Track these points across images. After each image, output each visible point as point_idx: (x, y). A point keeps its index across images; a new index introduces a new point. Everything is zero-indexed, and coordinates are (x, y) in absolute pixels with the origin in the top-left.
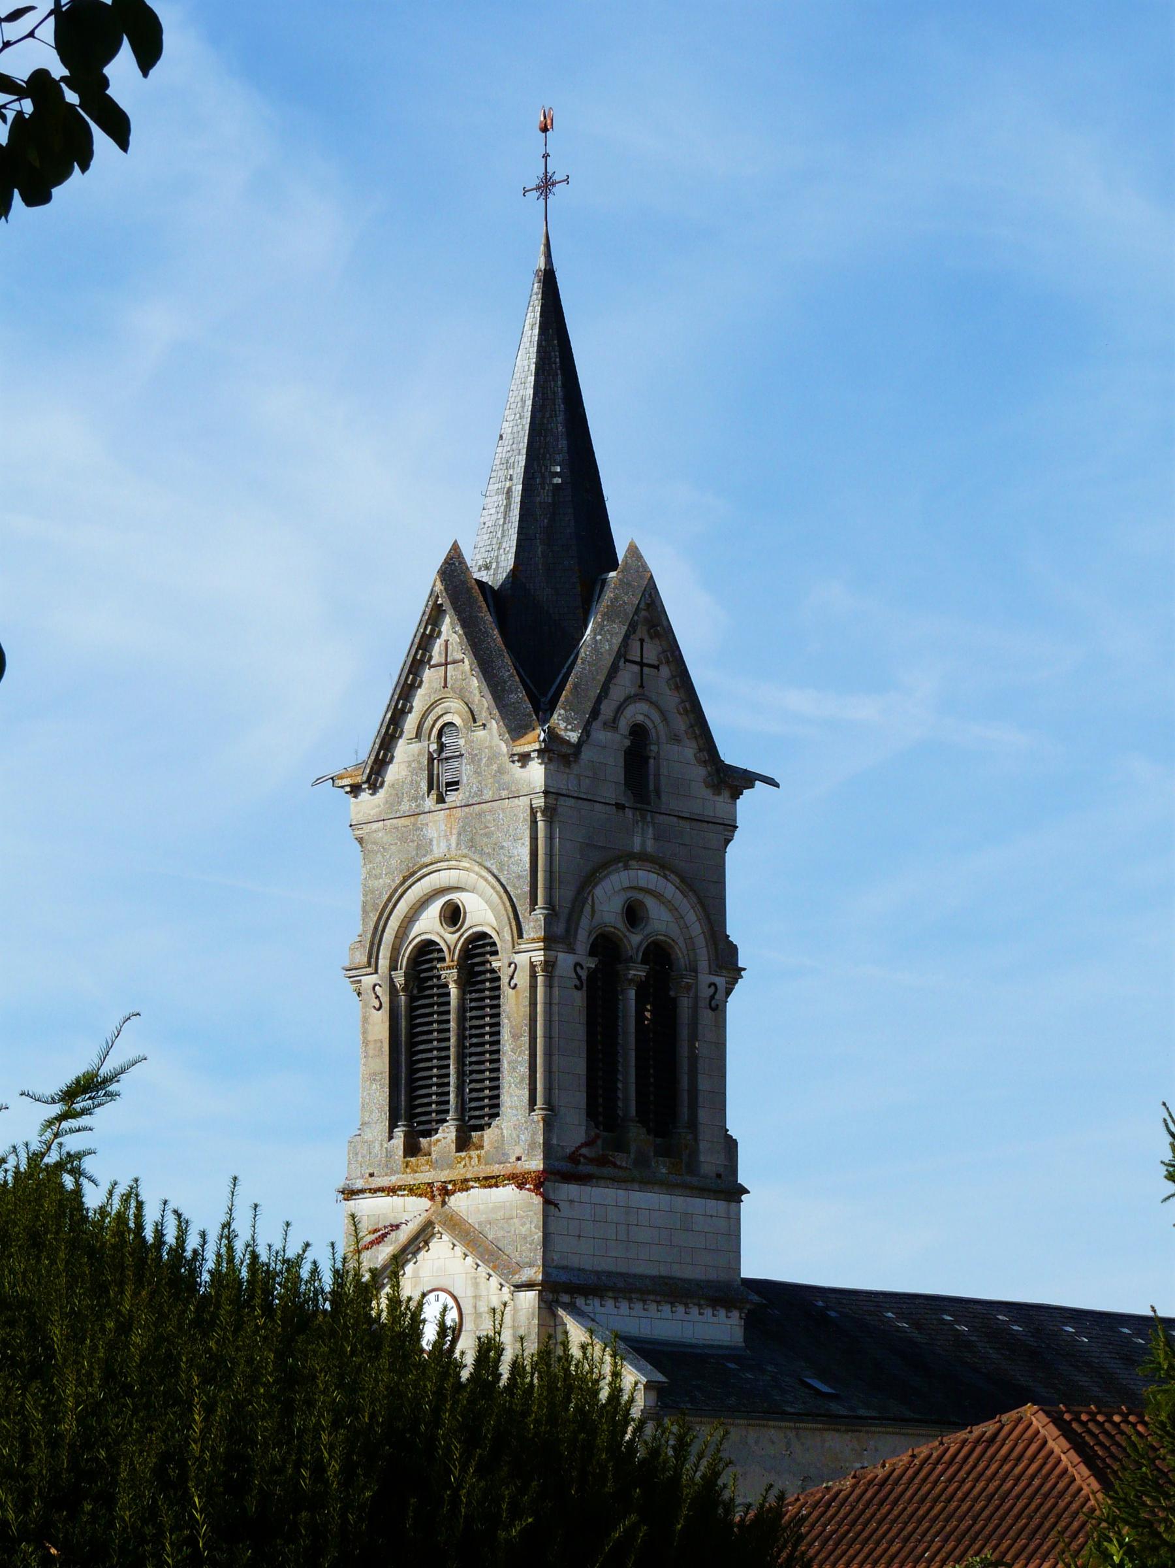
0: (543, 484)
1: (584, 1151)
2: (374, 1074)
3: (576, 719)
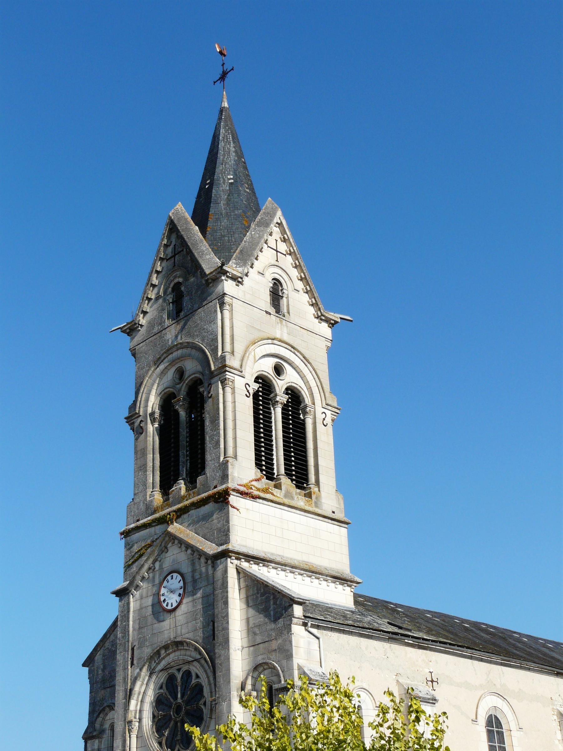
0: (224, 183)
1: (254, 483)
2: (140, 467)
3: (241, 263)
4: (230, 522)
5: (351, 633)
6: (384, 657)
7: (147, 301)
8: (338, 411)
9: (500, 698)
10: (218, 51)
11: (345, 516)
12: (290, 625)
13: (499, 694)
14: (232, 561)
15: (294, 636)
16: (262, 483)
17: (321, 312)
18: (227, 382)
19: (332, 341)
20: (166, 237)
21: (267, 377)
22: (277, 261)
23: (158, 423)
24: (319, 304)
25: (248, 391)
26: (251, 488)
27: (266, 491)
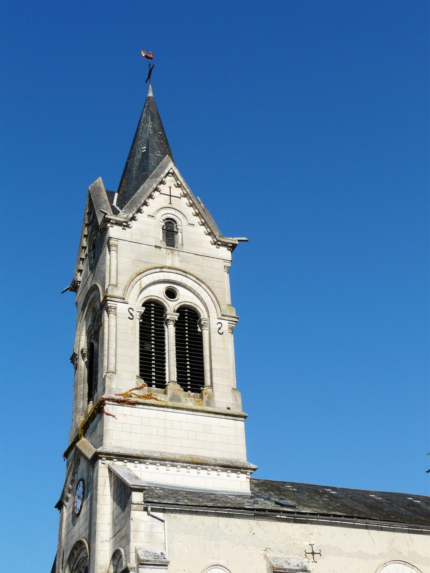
4: (104, 428)
5: (206, 514)
6: (249, 533)
7: (81, 261)
8: (236, 320)
9: (408, 566)
10: (144, 55)
11: (243, 411)
12: (130, 512)
13: (405, 562)
14: (103, 462)
15: (132, 521)
16: (144, 390)
17: (216, 238)
18: (109, 309)
19: (231, 261)
20: (88, 206)
21: (157, 300)
22: (170, 203)
23: (87, 358)
24: (214, 232)
25: (131, 314)
26: (131, 397)
27: (149, 397)
